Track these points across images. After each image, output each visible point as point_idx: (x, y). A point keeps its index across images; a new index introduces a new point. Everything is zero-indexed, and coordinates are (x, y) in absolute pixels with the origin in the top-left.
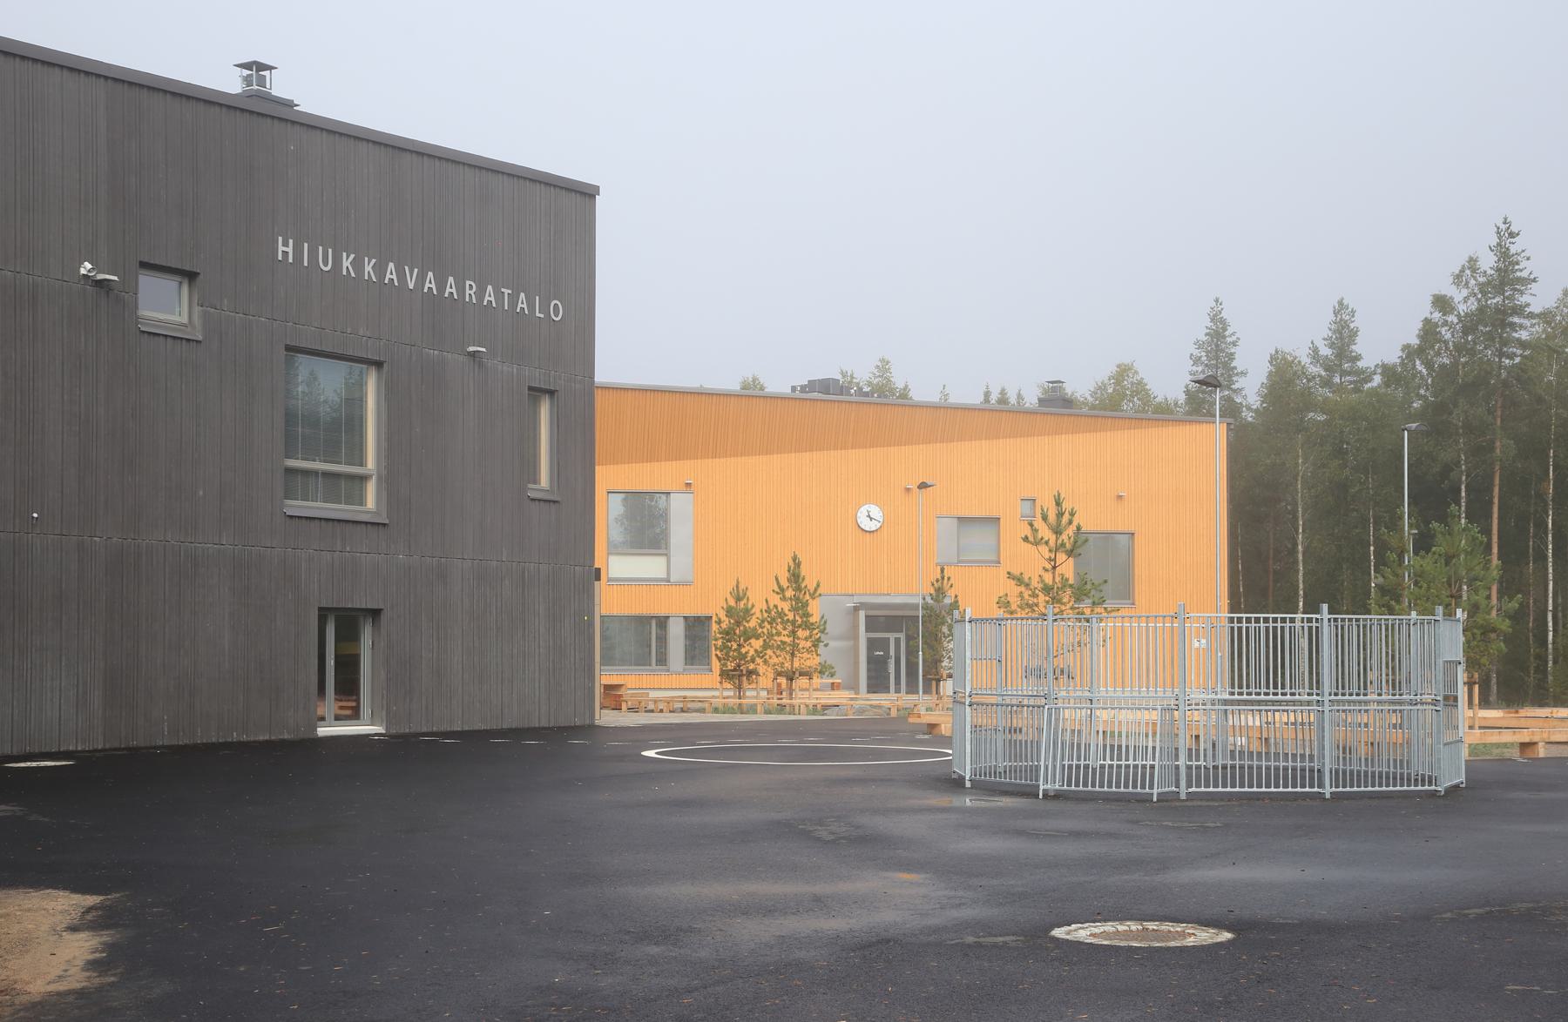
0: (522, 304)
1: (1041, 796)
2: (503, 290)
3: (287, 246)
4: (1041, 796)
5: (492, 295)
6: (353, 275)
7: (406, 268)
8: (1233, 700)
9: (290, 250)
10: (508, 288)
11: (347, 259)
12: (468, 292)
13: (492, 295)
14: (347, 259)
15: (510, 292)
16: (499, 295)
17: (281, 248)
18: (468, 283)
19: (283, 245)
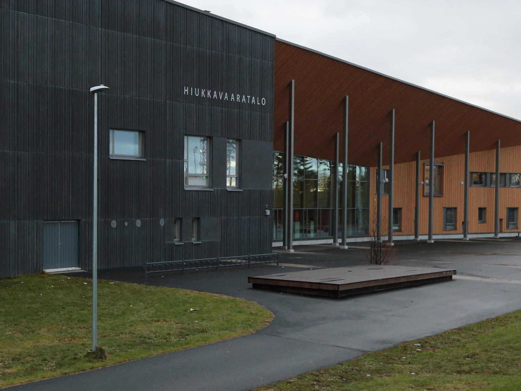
0: (253, 101)
1: (341, 208)
2: (248, 96)
3: (187, 89)
4: (341, 208)
5: (244, 99)
6: (239, 101)
7: (219, 92)
8: (330, 237)
9: (187, 91)
10: (249, 96)
11: (209, 92)
12: (237, 98)
13: (244, 99)
14: (209, 92)
15: (250, 97)
16: (246, 98)
17: (185, 90)
18: (238, 95)
19: (187, 92)
